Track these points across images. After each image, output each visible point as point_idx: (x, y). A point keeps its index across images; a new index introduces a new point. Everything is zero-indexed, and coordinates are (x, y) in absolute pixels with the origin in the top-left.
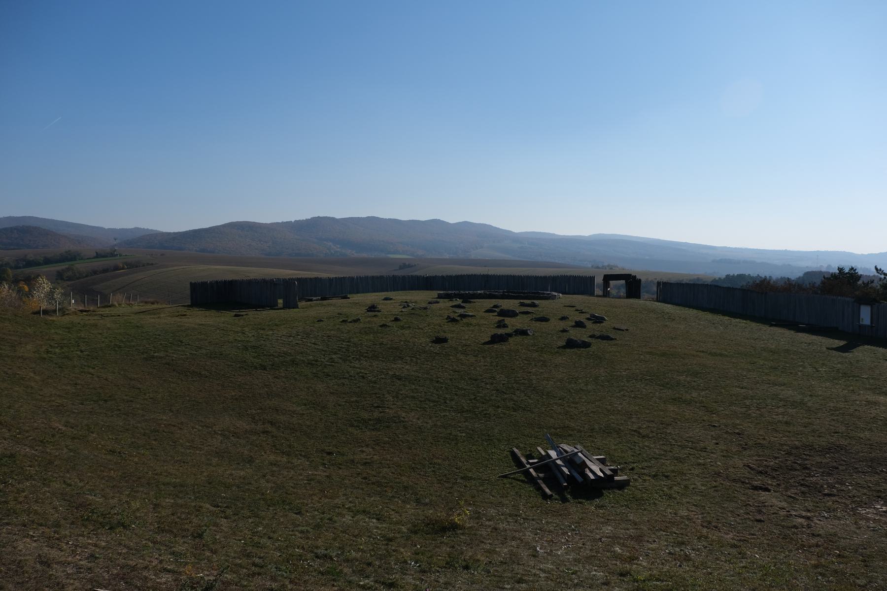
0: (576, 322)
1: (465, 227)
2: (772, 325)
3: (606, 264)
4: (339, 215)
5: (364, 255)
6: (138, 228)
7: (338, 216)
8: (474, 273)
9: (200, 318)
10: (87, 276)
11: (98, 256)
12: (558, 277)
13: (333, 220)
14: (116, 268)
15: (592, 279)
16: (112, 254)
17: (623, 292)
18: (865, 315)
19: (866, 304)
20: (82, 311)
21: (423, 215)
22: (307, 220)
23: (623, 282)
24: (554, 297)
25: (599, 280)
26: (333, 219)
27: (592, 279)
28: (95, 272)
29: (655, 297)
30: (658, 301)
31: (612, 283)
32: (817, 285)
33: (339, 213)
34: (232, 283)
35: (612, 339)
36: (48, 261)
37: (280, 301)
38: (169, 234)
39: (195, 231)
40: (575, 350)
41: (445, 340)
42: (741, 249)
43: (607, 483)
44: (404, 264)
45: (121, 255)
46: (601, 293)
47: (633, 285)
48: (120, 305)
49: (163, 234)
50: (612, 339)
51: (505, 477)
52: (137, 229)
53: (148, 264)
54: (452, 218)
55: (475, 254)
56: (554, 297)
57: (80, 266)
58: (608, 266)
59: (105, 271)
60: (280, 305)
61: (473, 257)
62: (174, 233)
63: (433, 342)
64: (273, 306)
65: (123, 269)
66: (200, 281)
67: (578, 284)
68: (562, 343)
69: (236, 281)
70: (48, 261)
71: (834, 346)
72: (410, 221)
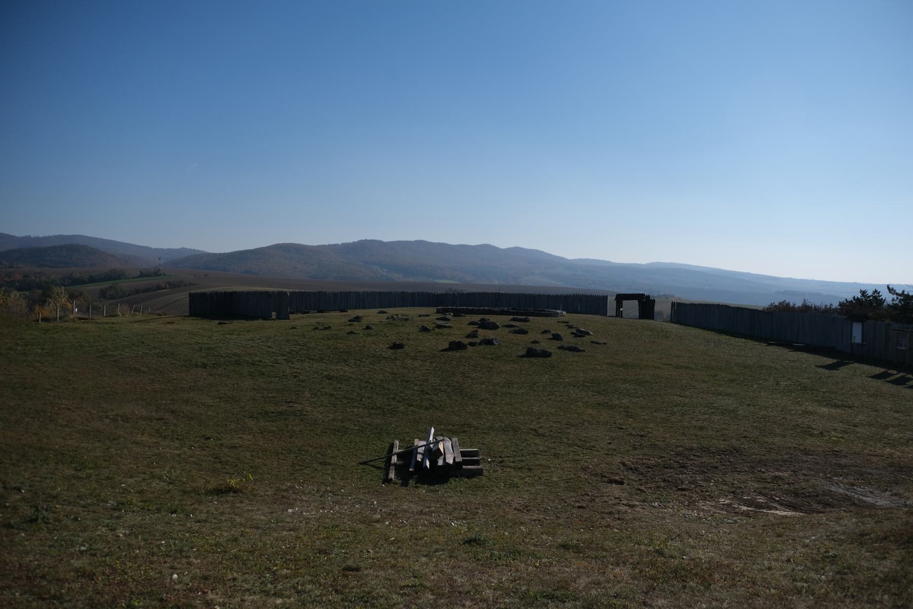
0: (553, 335)
2: (770, 345)
3: (662, 293)
4: (386, 239)
7: (385, 240)
8: (485, 291)
9: (209, 330)
10: (129, 295)
11: (143, 275)
12: (570, 296)
13: (380, 243)
14: (159, 288)
15: (605, 298)
16: (157, 273)
17: (636, 313)
18: (857, 332)
19: (857, 321)
20: (80, 319)
21: (473, 240)
22: (354, 243)
23: (636, 302)
24: (556, 315)
25: (611, 301)
26: (380, 243)
27: (605, 298)
28: (137, 292)
30: (672, 321)
31: (625, 303)
32: (834, 307)
33: (388, 235)
34: (232, 295)
35: (580, 351)
36: (92, 280)
37: (274, 313)
38: (215, 255)
39: (241, 253)
40: (533, 360)
41: (400, 346)
42: (807, 280)
43: (454, 471)
45: (164, 275)
46: (614, 313)
47: (646, 305)
49: (208, 255)
50: (580, 351)
51: (365, 463)
52: (183, 250)
53: (190, 284)
54: (503, 243)
56: (556, 315)
57: (123, 285)
58: (664, 295)
59: (147, 290)
60: (274, 317)
61: (523, 284)
62: (220, 254)
63: (391, 348)
64: (267, 317)
67: (592, 304)
68: (523, 352)
70: (92, 280)
71: (820, 364)
72: (459, 245)
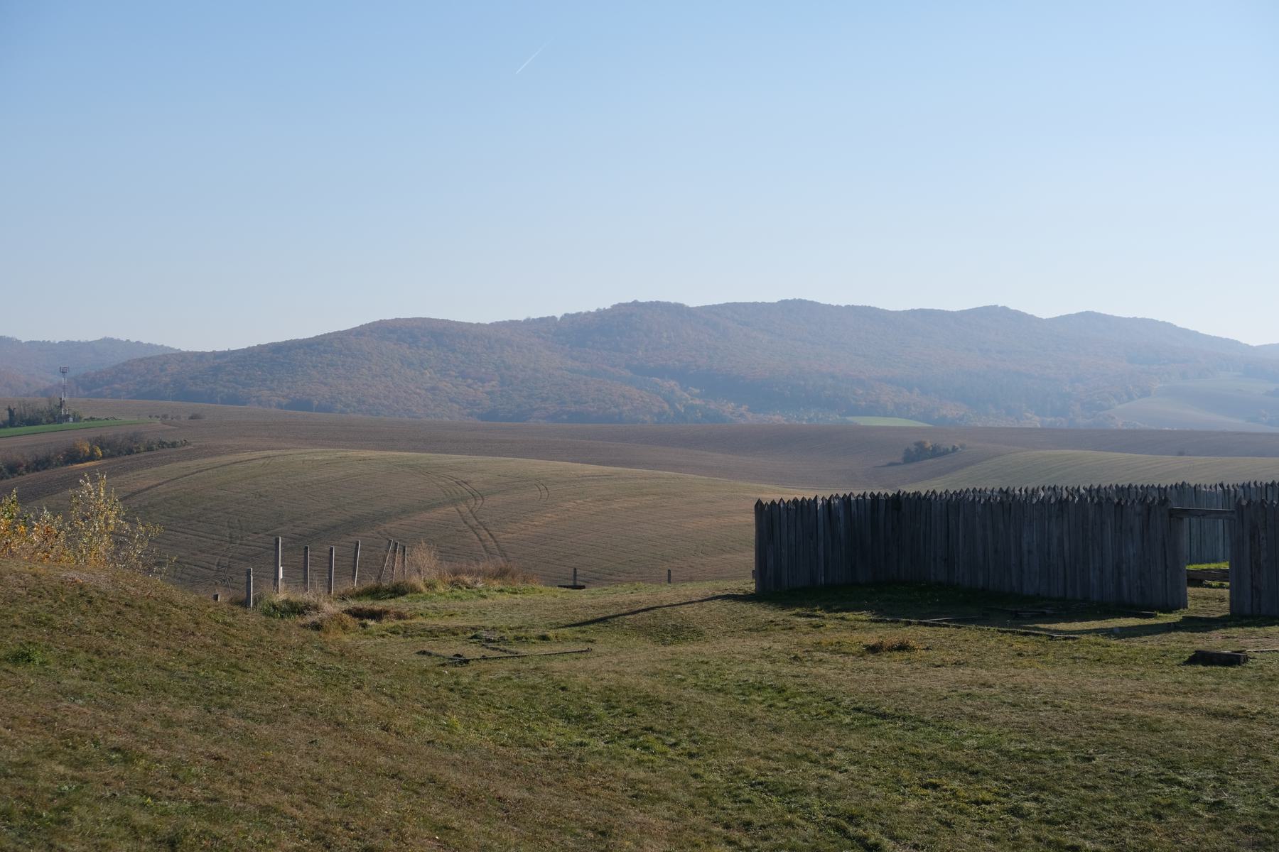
1: (1088, 325)
5: (777, 418)
6: (620, 305)
7: (693, 301)
9: (842, 654)
14: (73, 456)
21: (954, 295)
22: (600, 314)
26: (678, 309)
29: (751, 587)
34: (897, 502)
38: (202, 356)
39: (277, 348)
44: (920, 445)
45: (77, 419)
48: (430, 586)
49: (183, 357)
53: (162, 444)
55: (1127, 414)
59: (41, 464)
61: (1119, 423)
62: (216, 355)
65: (91, 457)
66: (1084, 485)
69: (918, 501)
